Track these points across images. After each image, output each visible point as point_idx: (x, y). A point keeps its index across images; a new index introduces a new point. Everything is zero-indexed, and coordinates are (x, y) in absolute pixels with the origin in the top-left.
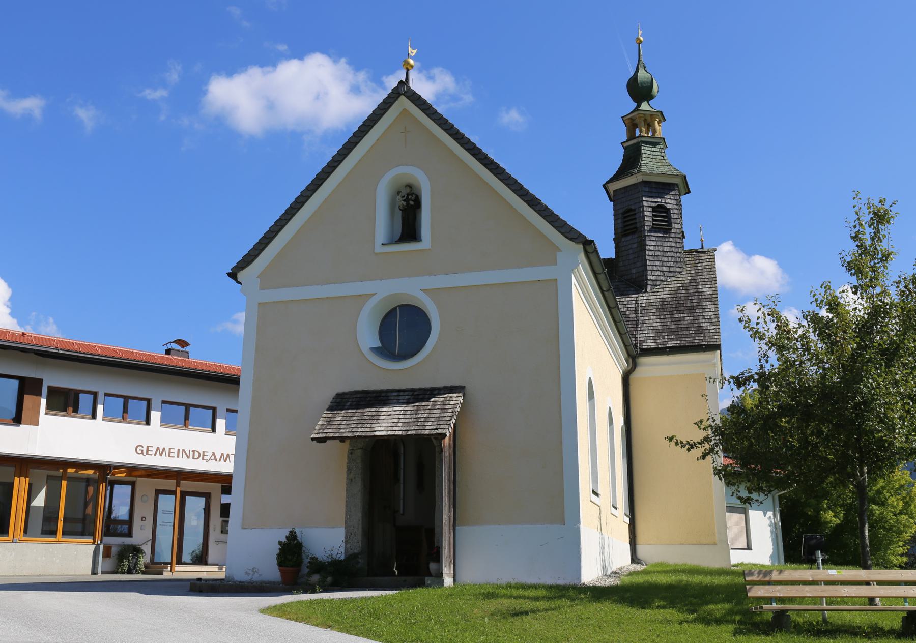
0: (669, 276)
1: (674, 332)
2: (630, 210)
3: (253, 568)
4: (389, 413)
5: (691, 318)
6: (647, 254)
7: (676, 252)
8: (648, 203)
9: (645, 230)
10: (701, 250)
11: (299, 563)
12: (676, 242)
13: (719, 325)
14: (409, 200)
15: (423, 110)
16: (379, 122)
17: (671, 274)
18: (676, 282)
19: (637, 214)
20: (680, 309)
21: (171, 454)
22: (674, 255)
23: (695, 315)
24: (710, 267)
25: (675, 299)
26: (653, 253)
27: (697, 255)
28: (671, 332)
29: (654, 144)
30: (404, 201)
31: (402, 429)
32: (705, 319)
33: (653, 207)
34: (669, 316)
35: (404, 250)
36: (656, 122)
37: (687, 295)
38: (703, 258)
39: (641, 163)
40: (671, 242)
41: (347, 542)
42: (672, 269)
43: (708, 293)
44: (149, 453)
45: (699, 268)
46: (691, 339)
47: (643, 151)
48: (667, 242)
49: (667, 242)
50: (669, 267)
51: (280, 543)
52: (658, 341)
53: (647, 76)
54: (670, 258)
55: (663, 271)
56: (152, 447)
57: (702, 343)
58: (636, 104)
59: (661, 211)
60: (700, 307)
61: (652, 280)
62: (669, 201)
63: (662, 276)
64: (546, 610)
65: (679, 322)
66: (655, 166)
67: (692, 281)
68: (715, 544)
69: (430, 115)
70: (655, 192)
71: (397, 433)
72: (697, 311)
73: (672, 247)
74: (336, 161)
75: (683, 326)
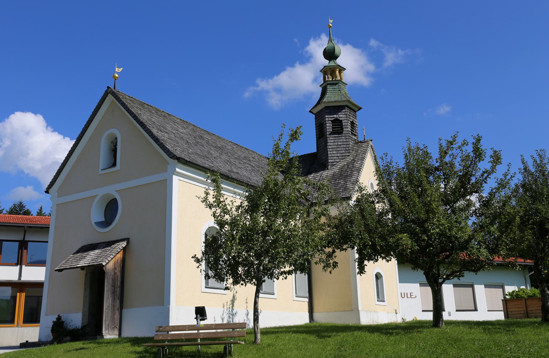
0: (342, 159)
3: (48, 335)
6: (328, 147)
7: (346, 144)
8: (329, 119)
12: (346, 139)
16: (101, 109)
17: (343, 157)
21: (412, 296)
22: (344, 146)
26: (332, 147)
33: (332, 121)
35: (113, 170)
42: (343, 155)
44: (412, 297)
50: (342, 153)
51: (53, 322)
55: (338, 156)
56: (412, 293)
59: (337, 123)
61: (331, 162)
63: (338, 159)
68: (352, 310)
70: (333, 112)
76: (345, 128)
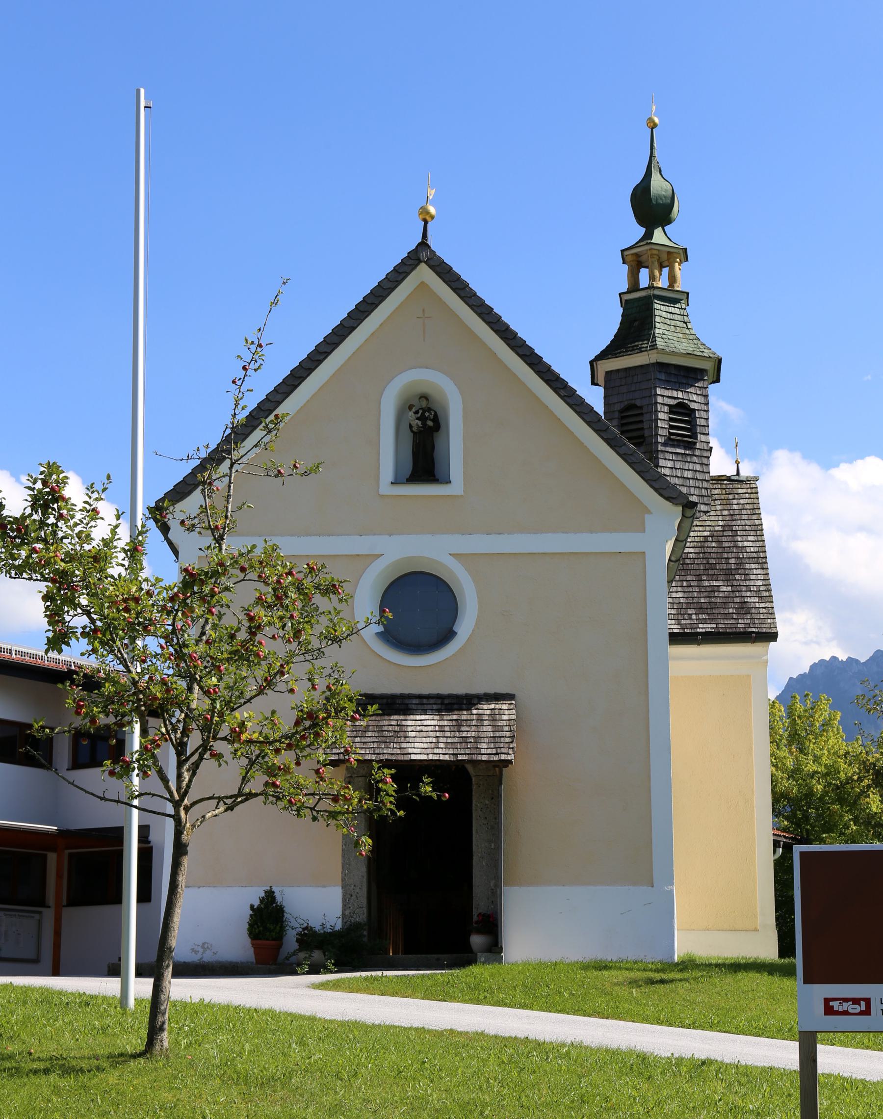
1: (708, 609)
2: (634, 407)
3: (204, 944)
4: (418, 728)
5: (729, 589)
7: (702, 480)
8: (665, 396)
9: (657, 442)
10: (736, 478)
11: (279, 937)
13: (772, 602)
14: (426, 419)
15: (455, 290)
18: (701, 528)
19: (645, 415)
20: (711, 572)
23: (735, 583)
24: (751, 506)
25: (701, 555)
27: (731, 486)
28: (701, 608)
29: (674, 301)
30: (418, 419)
31: (447, 752)
32: (751, 591)
33: (670, 406)
34: (695, 583)
36: (677, 264)
37: (720, 550)
38: (740, 491)
39: (654, 333)
40: (695, 463)
41: (345, 906)
43: (752, 550)
45: (735, 507)
46: (733, 621)
47: (657, 313)
48: (689, 462)
49: (689, 462)
52: (683, 622)
53: (664, 187)
54: (692, 489)
57: (750, 630)
58: (644, 229)
60: (742, 571)
62: (692, 397)
64: (681, 980)
65: (712, 594)
66: (675, 339)
67: (726, 528)
68: (756, 930)
69: (457, 290)
71: (442, 757)
72: (737, 577)
73: (696, 471)
74: (321, 353)
75: (717, 600)
76: (700, 433)
